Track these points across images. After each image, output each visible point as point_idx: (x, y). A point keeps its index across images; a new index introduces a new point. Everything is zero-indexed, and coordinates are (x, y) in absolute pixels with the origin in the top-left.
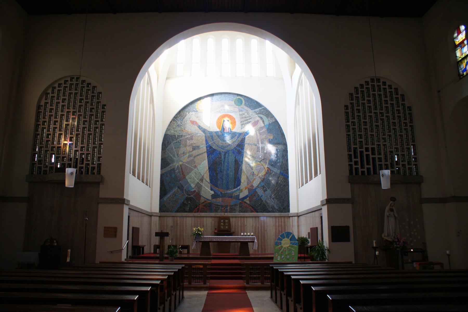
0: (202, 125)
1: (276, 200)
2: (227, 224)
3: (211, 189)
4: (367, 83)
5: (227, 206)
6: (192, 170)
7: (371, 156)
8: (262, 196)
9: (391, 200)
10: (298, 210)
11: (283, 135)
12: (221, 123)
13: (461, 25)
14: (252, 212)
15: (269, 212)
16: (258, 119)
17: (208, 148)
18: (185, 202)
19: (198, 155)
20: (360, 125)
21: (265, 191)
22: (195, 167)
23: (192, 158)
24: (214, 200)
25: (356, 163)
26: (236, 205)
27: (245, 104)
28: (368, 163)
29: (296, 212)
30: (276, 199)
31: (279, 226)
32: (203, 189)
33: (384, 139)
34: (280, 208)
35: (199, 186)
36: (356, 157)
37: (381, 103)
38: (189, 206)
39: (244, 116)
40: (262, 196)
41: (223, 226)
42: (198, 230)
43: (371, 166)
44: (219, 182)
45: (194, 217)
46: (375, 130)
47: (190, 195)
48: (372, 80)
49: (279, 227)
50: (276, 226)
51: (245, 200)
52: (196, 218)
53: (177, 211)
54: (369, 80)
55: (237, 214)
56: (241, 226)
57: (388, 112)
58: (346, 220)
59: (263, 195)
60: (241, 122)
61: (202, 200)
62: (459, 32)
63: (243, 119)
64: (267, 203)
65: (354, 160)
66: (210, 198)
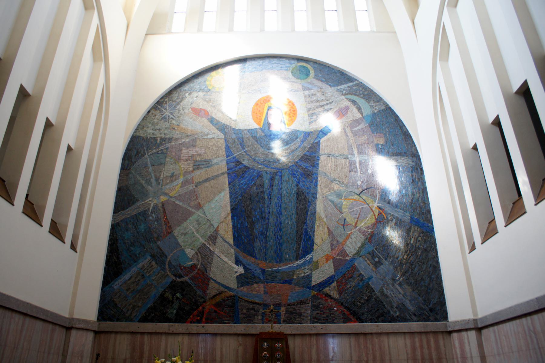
1: (409, 289)
2: (279, 355)
8: (370, 278)
14: (346, 320)
15: (393, 320)
18: (168, 295)
24: (245, 289)
30: (409, 284)
38: (176, 305)
40: (370, 278)
47: (180, 276)
51: (327, 290)
53: (144, 319)
59: (374, 276)
64: (386, 296)
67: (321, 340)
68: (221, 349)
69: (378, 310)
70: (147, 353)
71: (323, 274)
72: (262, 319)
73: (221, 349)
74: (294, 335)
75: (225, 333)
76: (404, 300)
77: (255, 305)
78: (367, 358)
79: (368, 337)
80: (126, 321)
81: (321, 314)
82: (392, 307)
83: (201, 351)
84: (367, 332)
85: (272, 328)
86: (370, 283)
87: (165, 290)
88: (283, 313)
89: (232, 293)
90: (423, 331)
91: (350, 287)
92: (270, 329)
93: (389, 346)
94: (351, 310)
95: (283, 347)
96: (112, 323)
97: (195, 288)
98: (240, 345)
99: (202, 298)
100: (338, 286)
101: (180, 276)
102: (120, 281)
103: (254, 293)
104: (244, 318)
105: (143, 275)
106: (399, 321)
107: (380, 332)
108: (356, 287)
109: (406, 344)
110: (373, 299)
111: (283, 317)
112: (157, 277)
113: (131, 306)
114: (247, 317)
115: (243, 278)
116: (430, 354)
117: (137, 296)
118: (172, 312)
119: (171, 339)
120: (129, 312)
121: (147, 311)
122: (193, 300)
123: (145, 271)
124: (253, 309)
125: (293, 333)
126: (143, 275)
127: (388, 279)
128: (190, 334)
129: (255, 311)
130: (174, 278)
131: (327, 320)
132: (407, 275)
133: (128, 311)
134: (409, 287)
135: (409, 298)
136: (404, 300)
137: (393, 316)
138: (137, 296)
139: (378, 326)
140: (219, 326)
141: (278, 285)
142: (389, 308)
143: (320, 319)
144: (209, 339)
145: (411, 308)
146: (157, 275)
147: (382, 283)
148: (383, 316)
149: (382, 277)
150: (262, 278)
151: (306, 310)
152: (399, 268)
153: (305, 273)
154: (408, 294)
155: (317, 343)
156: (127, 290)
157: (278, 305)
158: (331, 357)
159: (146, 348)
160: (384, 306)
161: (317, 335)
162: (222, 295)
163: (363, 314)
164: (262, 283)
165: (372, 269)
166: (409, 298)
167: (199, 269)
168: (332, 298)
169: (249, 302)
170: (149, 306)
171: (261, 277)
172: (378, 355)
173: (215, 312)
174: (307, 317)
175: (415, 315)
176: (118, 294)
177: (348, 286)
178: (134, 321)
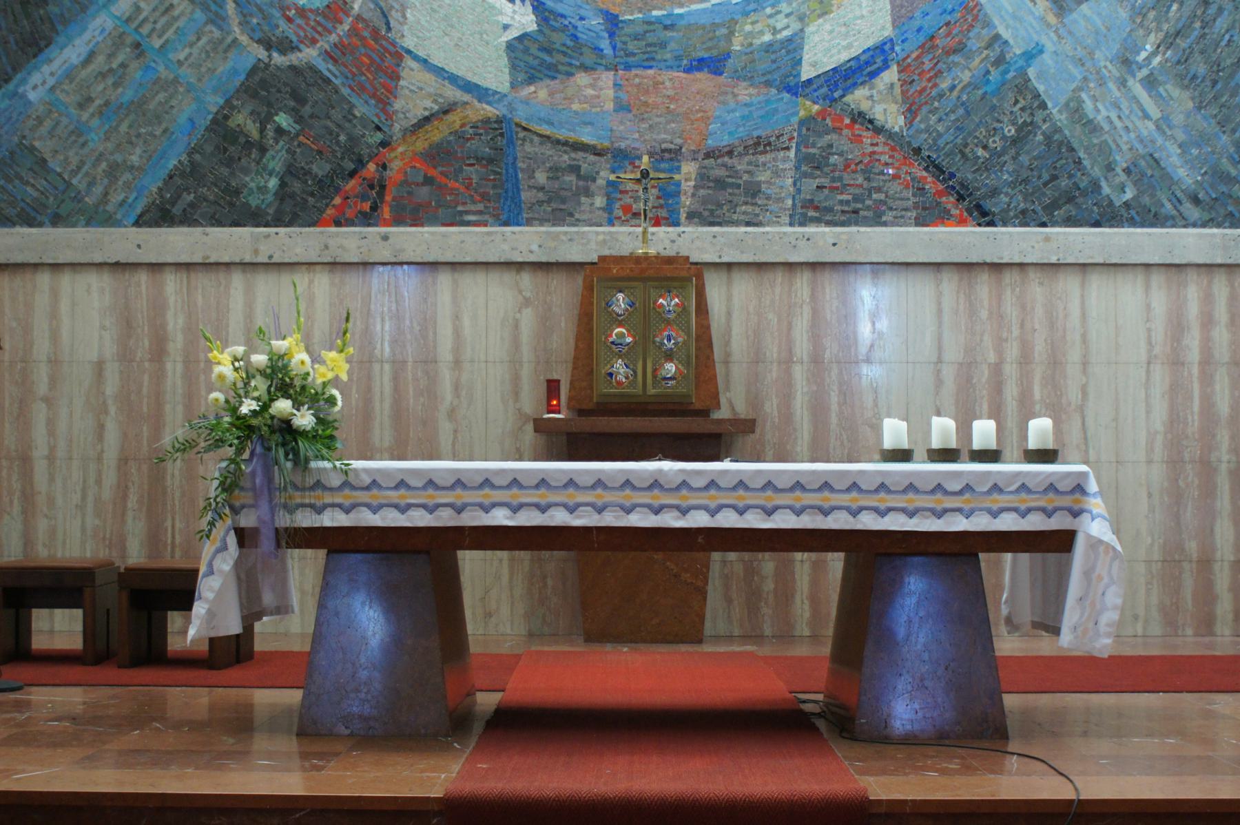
1: (1181, 100)
2: (670, 338)
8: (1030, 56)
14: (929, 215)
15: (1108, 217)
18: (242, 120)
24: (540, 92)
26: (760, 145)
30: (1188, 81)
31: (1207, 360)
38: (277, 159)
40: (1030, 56)
41: (628, 354)
42: (281, 380)
47: (286, 46)
49: (1207, 379)
50: (1176, 362)
51: (859, 97)
53: (161, 215)
55: (780, 238)
56: (816, 359)
59: (1049, 44)
61: (415, 95)
64: (1092, 127)
67: (830, 285)
68: (457, 318)
69: (1054, 178)
70: (180, 338)
71: (847, 35)
72: (608, 209)
73: (457, 318)
74: (729, 266)
75: (468, 259)
76: (1160, 141)
77: (581, 154)
78: (1000, 353)
79: (1009, 277)
80: (88, 224)
81: (832, 189)
82: (1110, 168)
83: (383, 329)
84: (1004, 261)
85: (645, 240)
86: (1031, 72)
87: (228, 102)
88: (688, 186)
89: (490, 110)
90: (1219, 261)
91: (953, 88)
92: (639, 243)
93: (1084, 316)
94: (952, 175)
95: (684, 309)
96: (34, 230)
97: (345, 91)
98: (527, 302)
99: (378, 128)
100: (904, 83)
101: (286, 46)
102: (46, 69)
103: (575, 107)
104: (540, 203)
105: (137, 45)
106: (1133, 223)
107: (1054, 260)
108: (976, 88)
109: (1148, 307)
110: (1040, 138)
111: (686, 201)
112: (195, 51)
113: (104, 165)
114: (549, 201)
115: (534, 50)
116: (1206, 534)
117: (124, 128)
118: (263, 184)
119: (265, 285)
120: (98, 190)
121: (166, 183)
122: (342, 138)
123: (145, 30)
124: (575, 169)
125: (725, 259)
126: (137, 45)
127: (1104, 58)
128: (334, 265)
129: (579, 177)
130: (262, 53)
131: (856, 212)
132: (1183, 43)
133: (91, 184)
134: (1186, 94)
135: (1181, 136)
136: (1160, 141)
137: (1111, 203)
138: (124, 128)
139: (1047, 239)
140: (444, 235)
141: (671, 79)
142: (1097, 172)
143: (829, 210)
144: (409, 281)
145: (1182, 172)
146: (191, 45)
147: (1077, 73)
148: (1071, 200)
149: (1080, 52)
150: (608, 51)
151: (777, 173)
152: (1152, 15)
153: (775, 31)
154: (1178, 119)
155: (813, 296)
156: (81, 106)
157: (669, 156)
158: (863, 350)
159: (175, 323)
160: (1079, 162)
161: (815, 266)
162: (455, 119)
163: (995, 192)
164: (607, 69)
165: (1042, 19)
166: (1181, 136)
167: (359, 18)
168: (879, 131)
169: (558, 142)
170: (173, 163)
171: (605, 45)
172: (1040, 348)
173: (428, 181)
174: (780, 200)
175: (1196, 201)
176: (48, 124)
177: (944, 85)
178: (118, 224)
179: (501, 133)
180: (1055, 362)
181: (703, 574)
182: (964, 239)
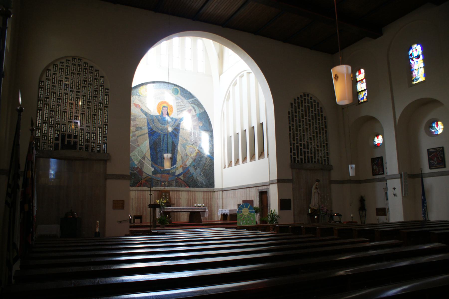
0: (144, 108)
1: (204, 178)
2: (168, 197)
3: (152, 167)
4: (301, 96)
5: (165, 181)
6: (136, 148)
7: (303, 150)
9: (317, 181)
10: (222, 186)
11: (210, 124)
12: (160, 109)
13: (362, 68)
14: (185, 187)
15: (199, 187)
16: (192, 108)
17: (150, 130)
19: (141, 135)
20: (296, 127)
21: (196, 169)
22: (138, 146)
23: (135, 138)
25: (294, 153)
26: (172, 181)
27: (181, 94)
28: (301, 155)
29: (221, 187)
30: (204, 176)
32: (145, 166)
33: (310, 138)
34: (207, 184)
35: (141, 163)
36: (294, 150)
37: (309, 112)
39: (180, 104)
43: (303, 157)
44: (159, 160)
45: (138, 190)
46: (305, 131)
47: (133, 171)
48: (304, 95)
50: (204, 199)
51: (180, 177)
52: (139, 192)
54: (302, 95)
56: (177, 199)
57: (313, 119)
58: (289, 195)
60: (177, 109)
61: (144, 176)
62: (360, 73)
63: (179, 107)
65: (293, 152)
66: (151, 174)
127: (199, 174)
179: (151, 179)
180: (195, 199)
181: (49, 162)
182: (188, 189)
